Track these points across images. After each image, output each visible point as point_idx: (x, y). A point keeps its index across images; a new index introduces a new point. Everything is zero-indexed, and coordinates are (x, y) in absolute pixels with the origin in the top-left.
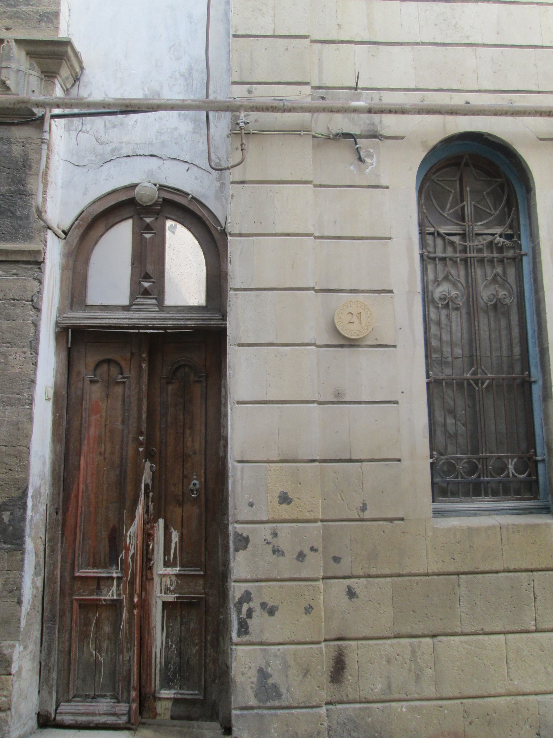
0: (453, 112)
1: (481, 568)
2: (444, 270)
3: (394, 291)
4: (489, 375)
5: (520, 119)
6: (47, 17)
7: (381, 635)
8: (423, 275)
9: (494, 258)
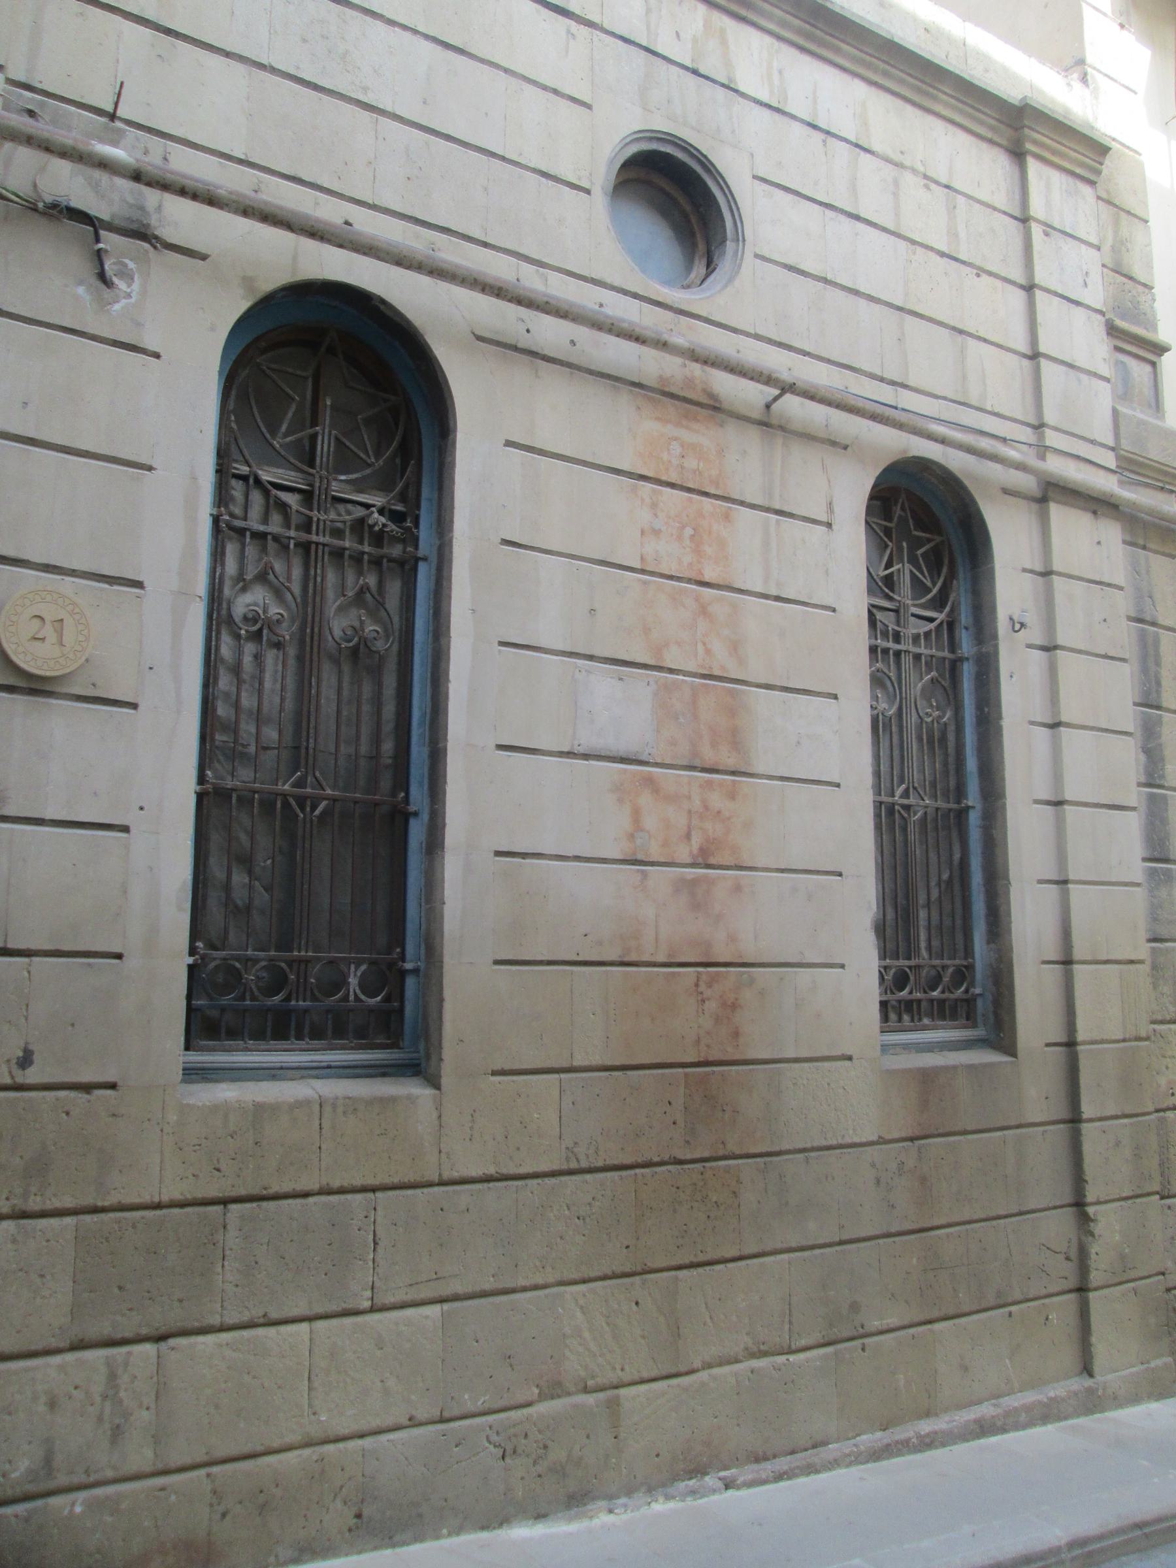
0: (315, 232)
1: (275, 1188)
2: (260, 559)
3: (146, 584)
4: (329, 792)
5: (444, 287)
7: (39, 1346)
8: (215, 561)
9: (363, 553)
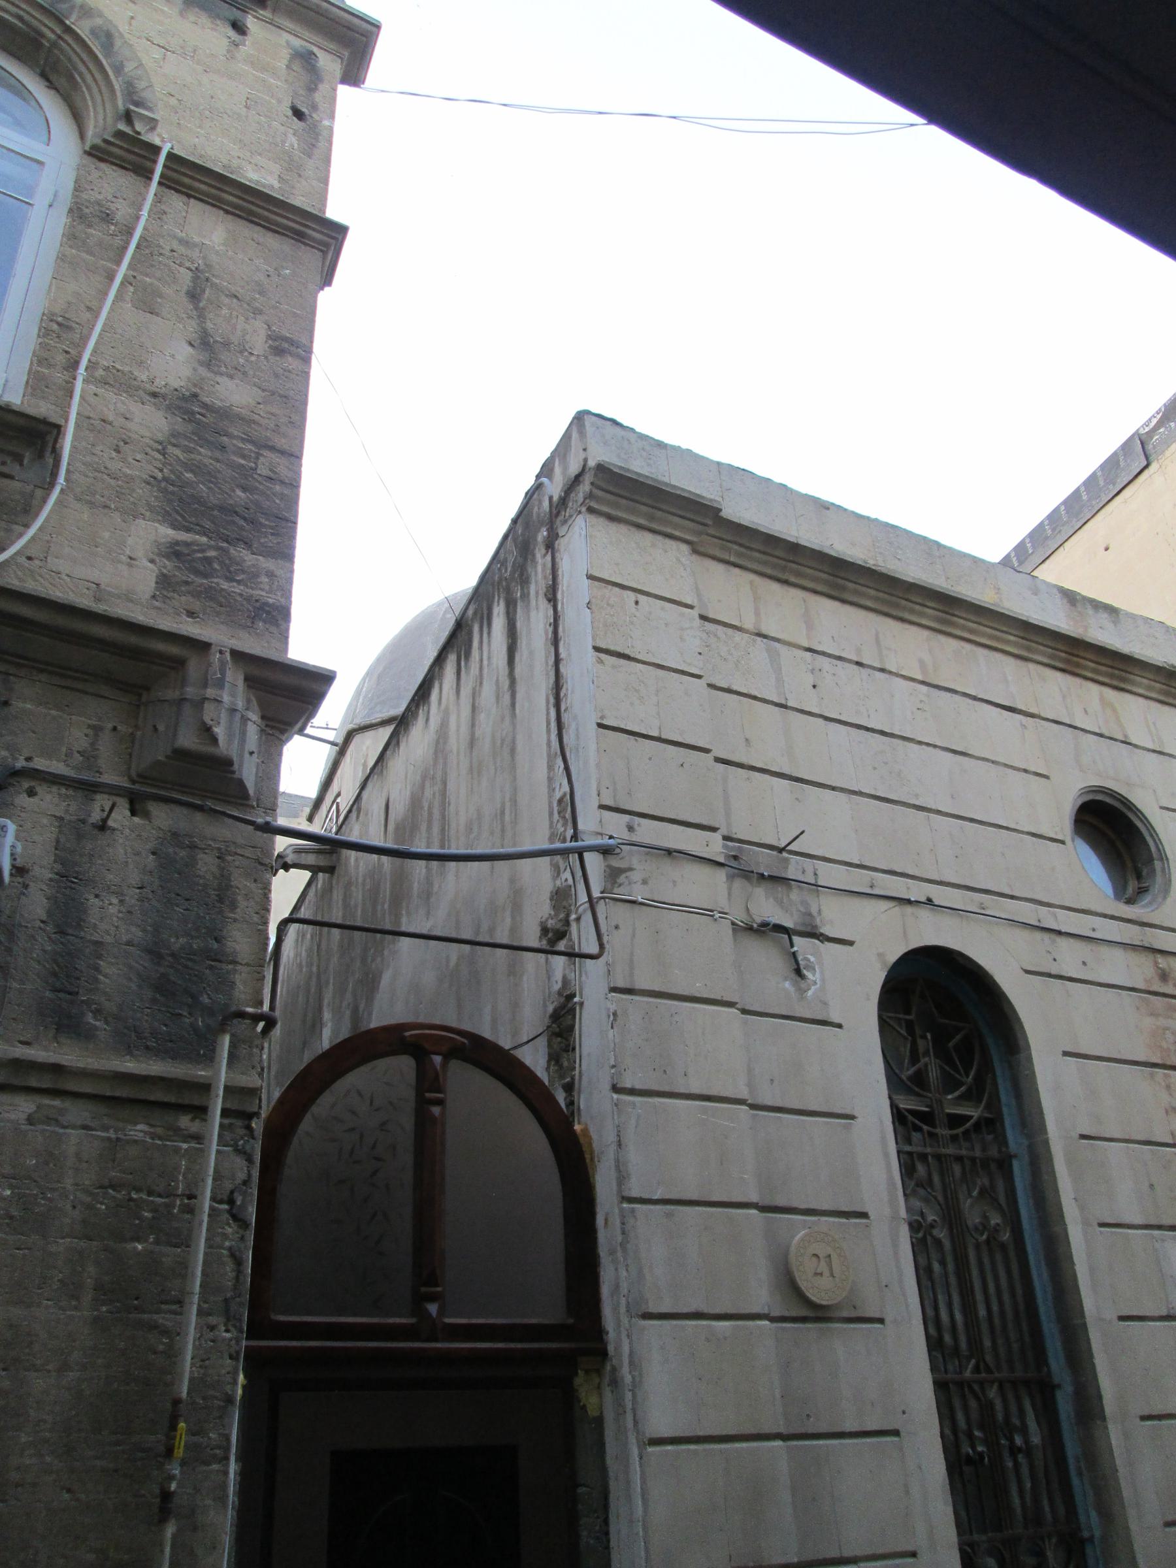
4: (997, 1375)
6: (268, 613)
